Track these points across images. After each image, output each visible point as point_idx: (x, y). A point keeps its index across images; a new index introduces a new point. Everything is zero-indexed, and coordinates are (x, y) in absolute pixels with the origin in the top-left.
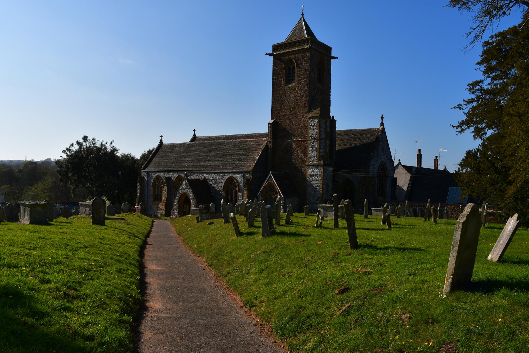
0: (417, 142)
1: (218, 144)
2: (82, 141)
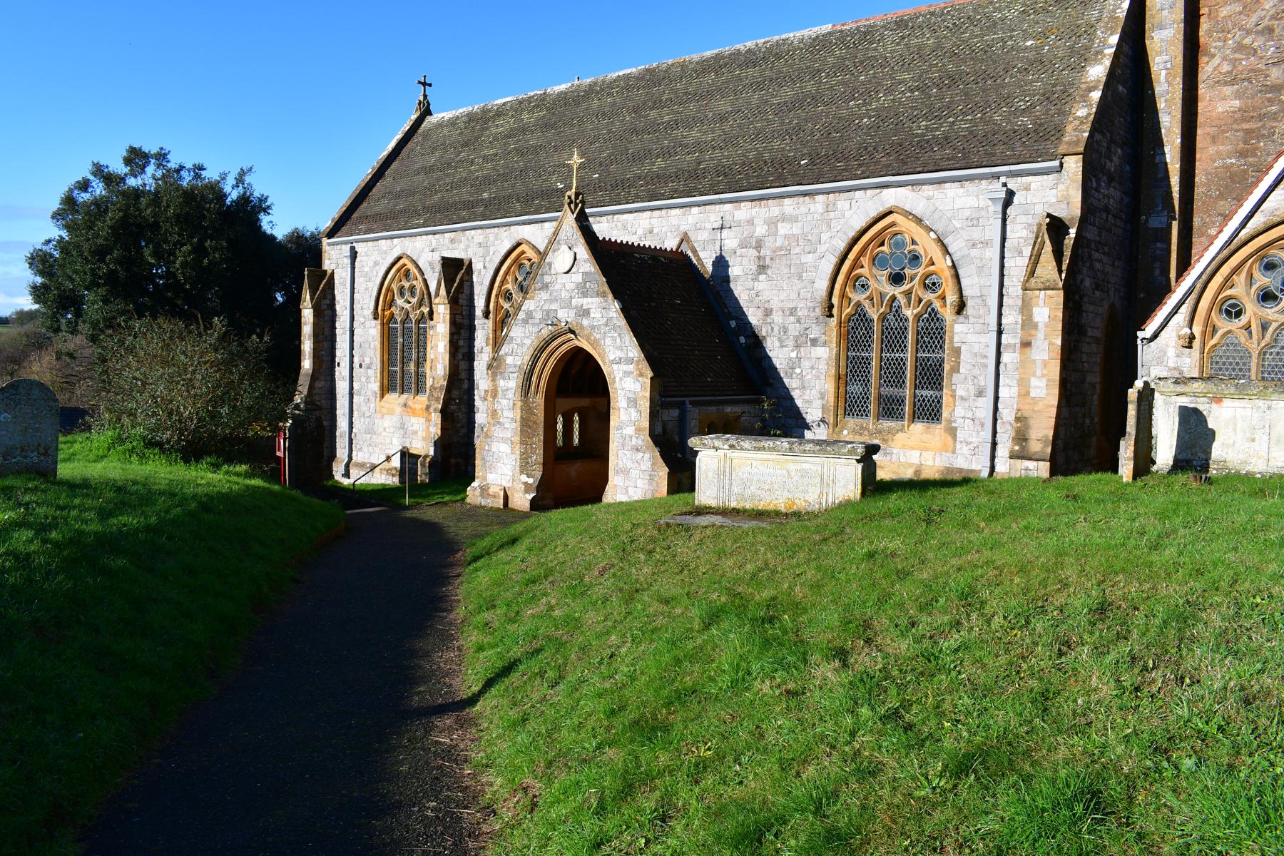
2: (119, 167)
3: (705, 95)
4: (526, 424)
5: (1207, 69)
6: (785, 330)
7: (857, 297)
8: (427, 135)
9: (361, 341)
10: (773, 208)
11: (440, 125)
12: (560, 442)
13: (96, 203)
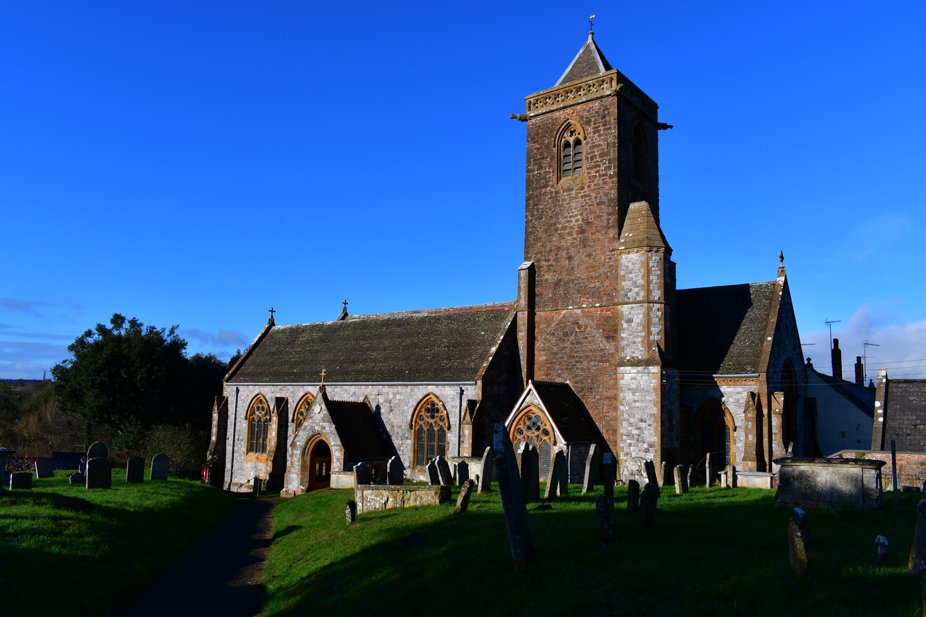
0: (828, 323)
2: (109, 326)
4: (303, 467)
5: (538, 345)
6: (398, 433)
7: (421, 423)
8: (272, 336)
9: (238, 428)
10: (395, 389)
11: (278, 332)
12: (317, 473)
13: (97, 343)
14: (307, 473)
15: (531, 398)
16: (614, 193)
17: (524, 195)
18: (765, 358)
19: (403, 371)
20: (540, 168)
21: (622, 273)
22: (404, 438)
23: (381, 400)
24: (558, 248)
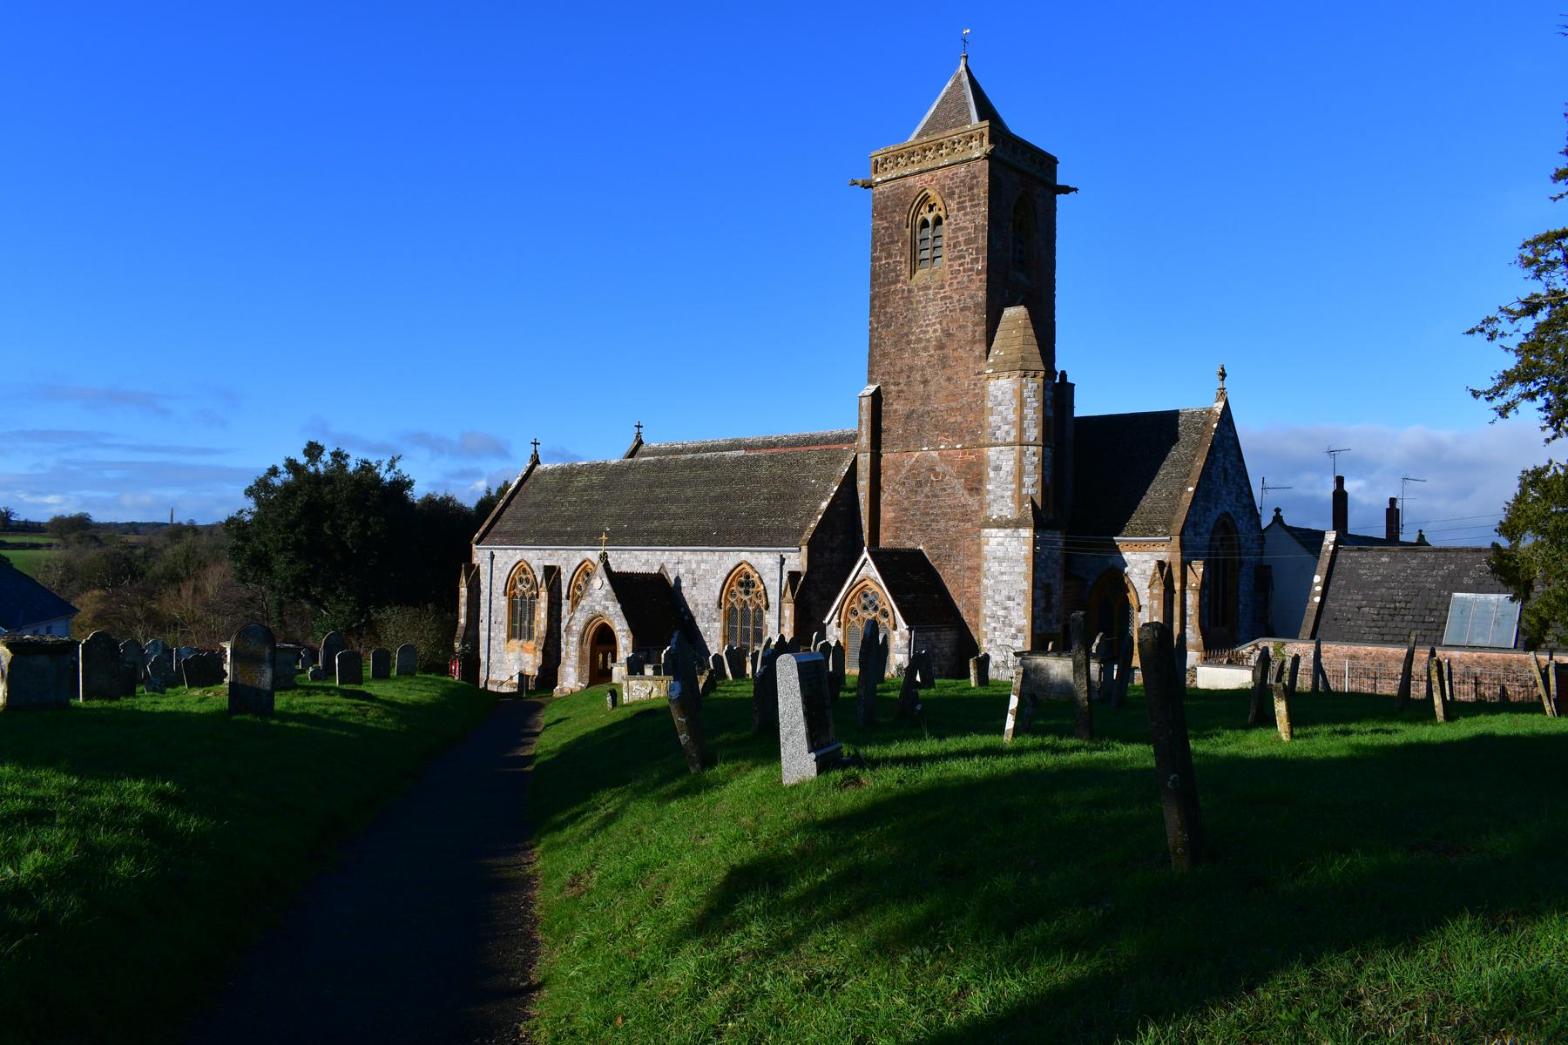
1: (707, 465)
2: (302, 460)
3: (682, 484)
4: (581, 659)
5: (884, 497)
8: (536, 479)
10: (699, 556)
11: (544, 473)
13: (286, 484)
14: (587, 667)
15: (867, 570)
16: (981, 295)
17: (868, 293)
18: (1182, 515)
19: (709, 532)
20: (889, 256)
21: (990, 405)
22: (712, 620)
23: (682, 571)
24: (911, 368)
